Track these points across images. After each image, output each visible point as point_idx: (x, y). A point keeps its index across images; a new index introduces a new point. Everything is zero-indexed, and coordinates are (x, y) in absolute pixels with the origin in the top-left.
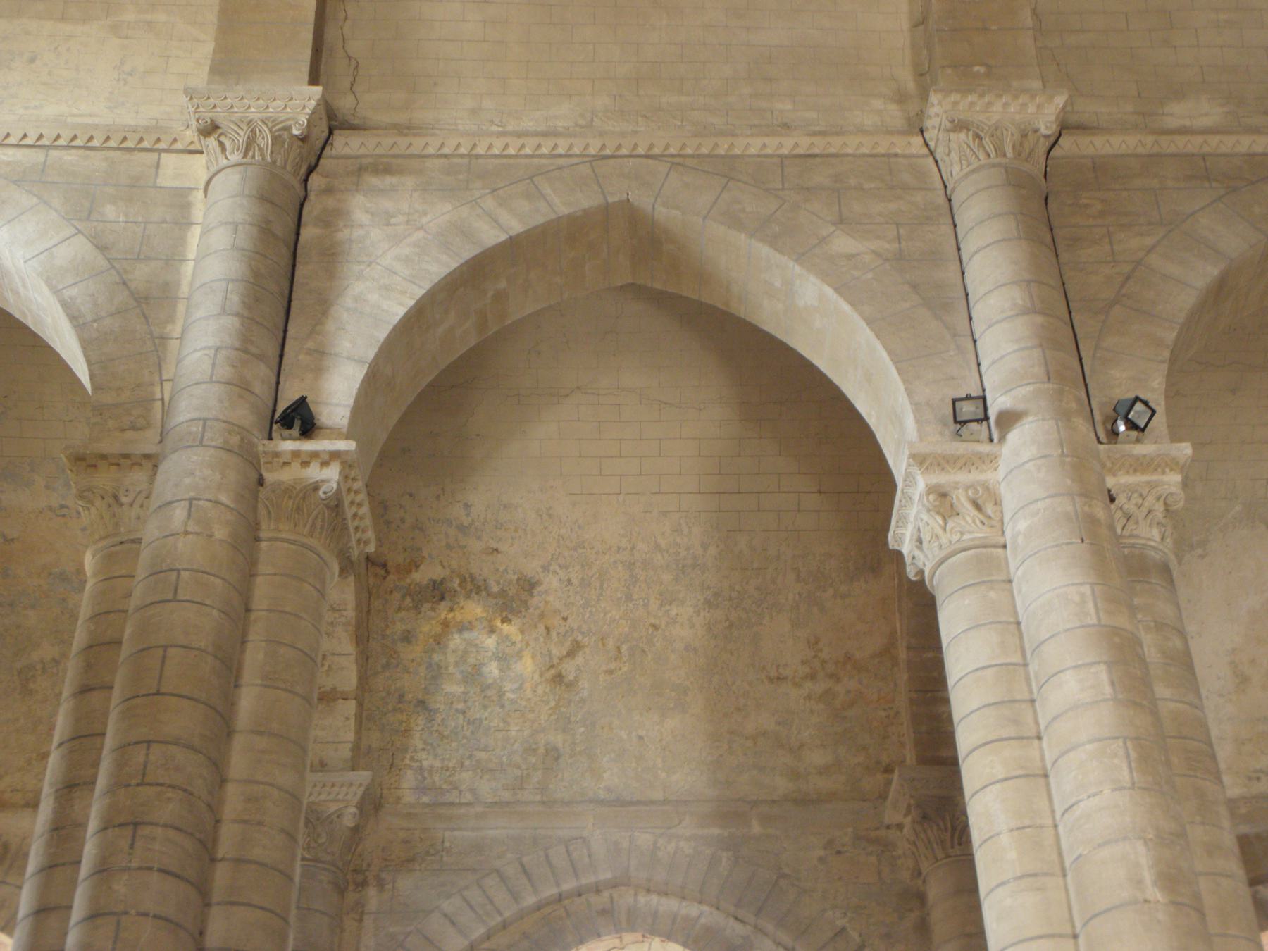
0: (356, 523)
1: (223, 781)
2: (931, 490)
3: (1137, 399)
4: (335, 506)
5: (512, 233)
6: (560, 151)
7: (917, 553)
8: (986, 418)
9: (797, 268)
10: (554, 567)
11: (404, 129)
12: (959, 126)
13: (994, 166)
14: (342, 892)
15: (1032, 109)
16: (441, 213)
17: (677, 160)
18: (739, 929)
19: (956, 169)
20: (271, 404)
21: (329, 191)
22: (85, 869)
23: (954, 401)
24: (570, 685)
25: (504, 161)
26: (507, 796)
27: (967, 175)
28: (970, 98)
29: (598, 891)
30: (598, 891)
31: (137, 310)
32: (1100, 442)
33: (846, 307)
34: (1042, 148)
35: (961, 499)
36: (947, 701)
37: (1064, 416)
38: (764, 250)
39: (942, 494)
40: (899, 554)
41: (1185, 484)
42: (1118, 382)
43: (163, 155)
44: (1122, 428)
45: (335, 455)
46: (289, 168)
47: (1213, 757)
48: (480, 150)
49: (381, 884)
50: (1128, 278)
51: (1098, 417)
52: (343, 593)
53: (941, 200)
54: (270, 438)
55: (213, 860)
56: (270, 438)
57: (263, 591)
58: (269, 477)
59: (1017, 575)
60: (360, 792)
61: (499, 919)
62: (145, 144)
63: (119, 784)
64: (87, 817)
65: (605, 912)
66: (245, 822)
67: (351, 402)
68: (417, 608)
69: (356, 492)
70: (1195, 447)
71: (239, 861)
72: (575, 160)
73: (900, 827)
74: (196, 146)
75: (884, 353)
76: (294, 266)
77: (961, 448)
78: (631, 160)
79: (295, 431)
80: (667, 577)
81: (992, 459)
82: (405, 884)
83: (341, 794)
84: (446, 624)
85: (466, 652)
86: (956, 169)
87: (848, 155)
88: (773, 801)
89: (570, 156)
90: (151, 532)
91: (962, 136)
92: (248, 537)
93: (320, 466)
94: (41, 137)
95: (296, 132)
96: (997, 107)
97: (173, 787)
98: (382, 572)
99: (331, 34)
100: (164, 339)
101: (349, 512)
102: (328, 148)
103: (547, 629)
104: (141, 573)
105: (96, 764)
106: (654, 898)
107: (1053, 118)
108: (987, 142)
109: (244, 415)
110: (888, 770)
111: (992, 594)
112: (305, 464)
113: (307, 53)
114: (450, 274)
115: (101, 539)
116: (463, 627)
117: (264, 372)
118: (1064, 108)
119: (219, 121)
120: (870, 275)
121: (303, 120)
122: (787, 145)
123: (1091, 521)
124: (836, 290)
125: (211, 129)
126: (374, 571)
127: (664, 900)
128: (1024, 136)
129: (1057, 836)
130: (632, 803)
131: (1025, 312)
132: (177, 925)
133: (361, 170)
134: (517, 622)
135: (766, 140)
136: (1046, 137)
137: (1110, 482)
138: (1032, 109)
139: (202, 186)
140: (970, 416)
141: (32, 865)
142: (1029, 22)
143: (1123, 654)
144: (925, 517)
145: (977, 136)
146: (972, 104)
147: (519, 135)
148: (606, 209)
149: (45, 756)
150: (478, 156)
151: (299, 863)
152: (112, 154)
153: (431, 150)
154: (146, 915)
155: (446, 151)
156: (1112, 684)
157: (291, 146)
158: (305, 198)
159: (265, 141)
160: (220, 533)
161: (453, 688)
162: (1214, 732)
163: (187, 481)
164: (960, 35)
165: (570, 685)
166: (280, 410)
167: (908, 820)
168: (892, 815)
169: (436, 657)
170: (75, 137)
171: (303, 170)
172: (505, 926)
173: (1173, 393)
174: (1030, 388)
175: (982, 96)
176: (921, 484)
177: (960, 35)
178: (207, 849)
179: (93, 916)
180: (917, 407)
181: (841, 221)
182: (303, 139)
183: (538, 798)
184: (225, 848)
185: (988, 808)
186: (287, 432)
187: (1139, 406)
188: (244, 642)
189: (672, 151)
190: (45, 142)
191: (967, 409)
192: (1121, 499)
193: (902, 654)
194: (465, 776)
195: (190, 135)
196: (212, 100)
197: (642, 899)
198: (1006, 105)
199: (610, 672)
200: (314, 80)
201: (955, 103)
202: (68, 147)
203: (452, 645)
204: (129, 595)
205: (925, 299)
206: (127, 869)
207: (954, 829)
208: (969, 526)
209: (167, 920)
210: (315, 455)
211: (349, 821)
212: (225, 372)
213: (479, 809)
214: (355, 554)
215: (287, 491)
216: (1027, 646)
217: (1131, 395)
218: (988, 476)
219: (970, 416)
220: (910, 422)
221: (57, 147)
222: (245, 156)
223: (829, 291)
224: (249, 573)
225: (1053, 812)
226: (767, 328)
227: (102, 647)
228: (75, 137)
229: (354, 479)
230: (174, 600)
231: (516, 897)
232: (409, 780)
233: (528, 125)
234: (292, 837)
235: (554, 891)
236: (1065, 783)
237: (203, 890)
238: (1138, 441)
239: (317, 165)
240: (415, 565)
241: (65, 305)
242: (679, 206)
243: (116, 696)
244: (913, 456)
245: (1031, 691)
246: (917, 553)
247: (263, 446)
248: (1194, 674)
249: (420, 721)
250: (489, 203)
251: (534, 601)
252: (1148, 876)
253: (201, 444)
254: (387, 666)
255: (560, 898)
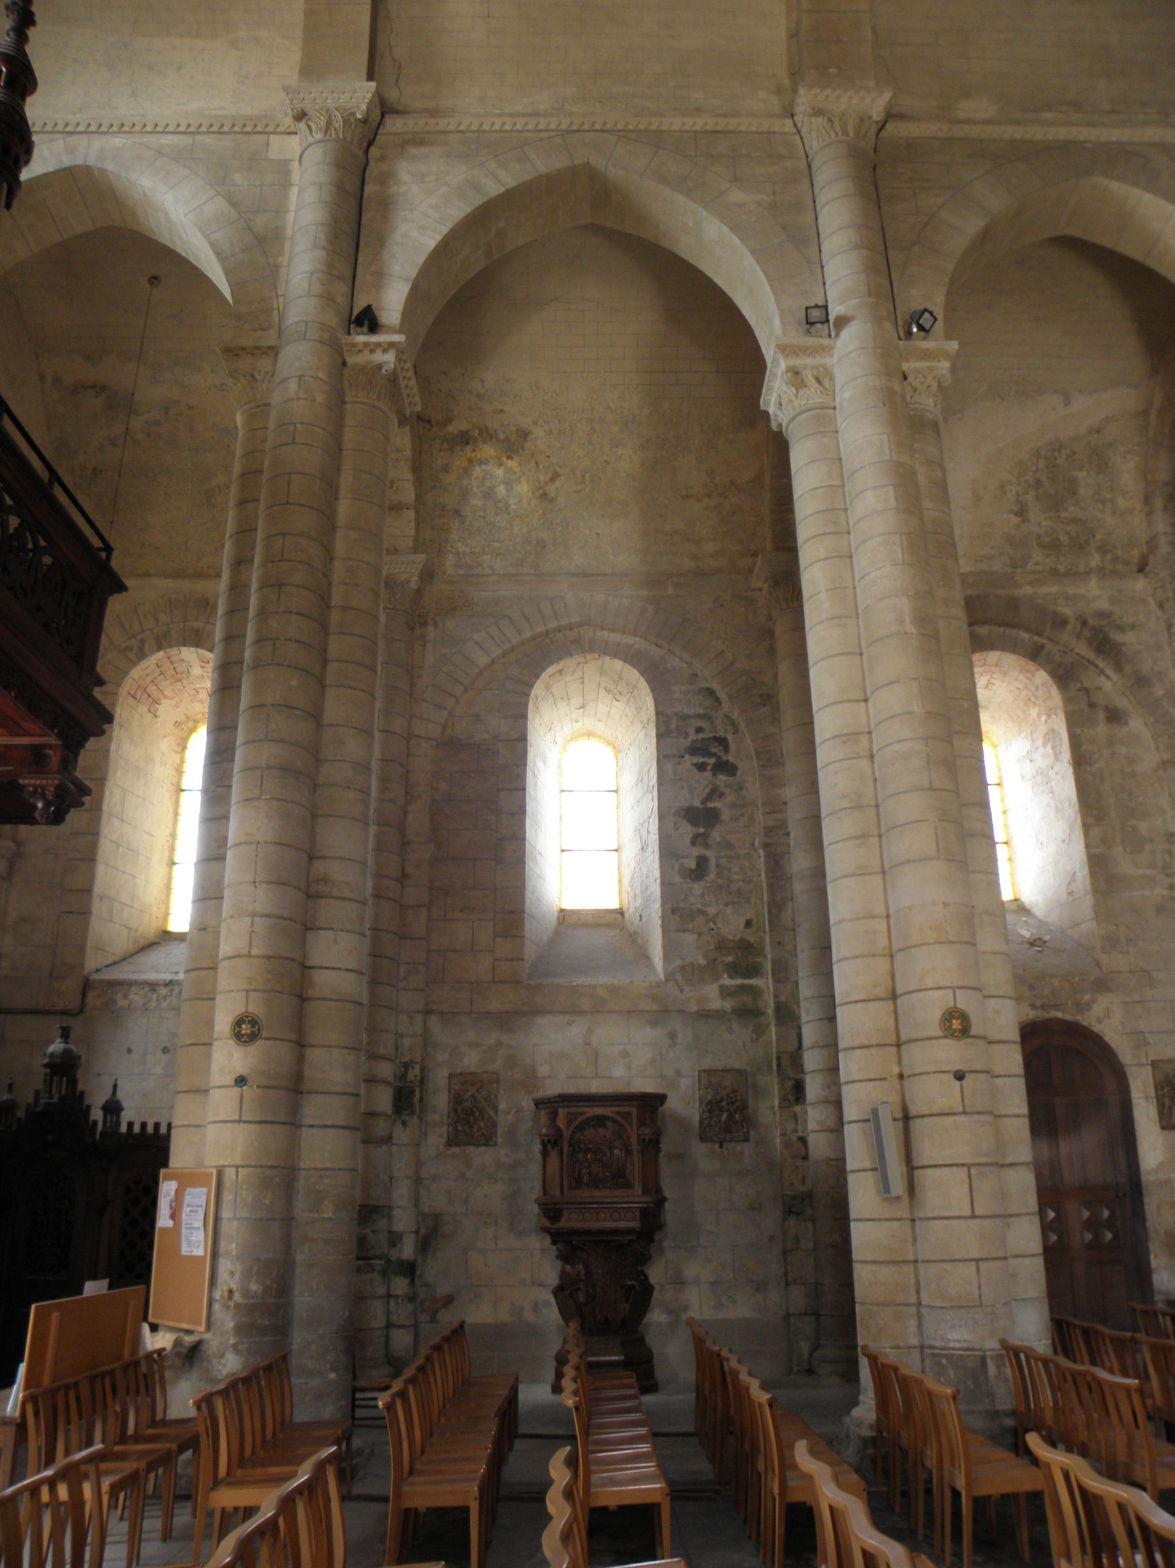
0: (408, 391)
1: (332, 559)
2: (789, 369)
3: (926, 310)
4: (393, 379)
5: (508, 187)
6: (541, 127)
7: (779, 413)
8: (827, 321)
9: (705, 213)
10: (541, 422)
11: (433, 113)
12: (818, 112)
13: (841, 142)
14: (412, 629)
15: (868, 101)
16: (459, 173)
17: (622, 134)
18: (658, 651)
19: (815, 144)
20: (348, 310)
21: (383, 158)
22: (252, 612)
23: (807, 308)
24: (552, 500)
25: (502, 135)
26: (512, 570)
27: (822, 149)
28: (827, 92)
29: (571, 629)
30: (571, 629)
31: (259, 246)
32: (900, 339)
33: (737, 241)
34: (873, 131)
35: (808, 376)
36: (792, 511)
37: (877, 320)
38: (683, 200)
39: (796, 373)
40: (767, 413)
41: (953, 370)
42: (914, 298)
43: (271, 136)
44: (915, 330)
45: (392, 345)
46: (355, 142)
47: (954, 546)
48: (486, 127)
49: (436, 625)
50: (925, 227)
51: (900, 322)
52: (402, 440)
53: (804, 166)
54: (349, 334)
55: (329, 607)
56: (349, 334)
57: (350, 437)
58: (350, 360)
59: (842, 426)
60: (420, 568)
61: (509, 645)
62: (259, 129)
63: (267, 561)
64: (251, 580)
65: (576, 641)
66: (346, 584)
67: (401, 308)
68: (451, 449)
69: (407, 370)
70: (960, 344)
71: (345, 608)
72: (553, 134)
73: (760, 590)
74: (293, 129)
75: (762, 274)
76: (360, 213)
77: (809, 341)
78: (591, 134)
79: (365, 329)
80: (615, 429)
81: (829, 349)
82: (450, 624)
83: (408, 569)
84: (470, 460)
85: (484, 479)
86: (815, 144)
87: (740, 132)
88: (682, 574)
89: (548, 131)
90: (276, 398)
91: (820, 120)
92: (338, 400)
93: (383, 351)
94: (189, 125)
95: (359, 116)
96: (845, 99)
97: (300, 562)
98: (428, 426)
99: (381, 44)
100: (277, 267)
101: (403, 383)
102: (381, 128)
103: (537, 463)
104: (272, 425)
105: (253, 549)
106: (606, 633)
107: (881, 108)
108: (836, 124)
109: (331, 318)
110: (755, 554)
111: (825, 440)
112: (372, 351)
113: (365, 57)
114: (466, 217)
115: (246, 404)
116: (481, 462)
117: (343, 288)
118: (889, 102)
119: (310, 111)
120: (754, 219)
121: (364, 107)
122: (699, 123)
123: (891, 392)
124: (731, 229)
125: (301, 116)
126: (422, 425)
127: (612, 634)
128: (862, 120)
129: (855, 593)
130: (592, 575)
131: (856, 248)
132: (310, 646)
133: (404, 144)
134: (516, 458)
135: (685, 120)
136: (877, 122)
137: (905, 366)
138: (868, 101)
139: (297, 157)
140: (817, 319)
141: (221, 611)
142: (870, 36)
143: (905, 481)
144: (784, 388)
145: (830, 120)
146: (827, 96)
147: (511, 115)
148: (573, 169)
149: (223, 546)
150: (484, 131)
151: (381, 610)
152: (237, 136)
153: (451, 128)
154: (290, 640)
155: (462, 128)
156: (896, 498)
157: (356, 126)
158: (367, 164)
159: (338, 123)
160: (320, 398)
161: (477, 502)
162: (957, 532)
163: (297, 364)
164: (820, 49)
165: (552, 500)
166: (356, 312)
167: (766, 586)
168: (756, 583)
169: (465, 482)
170: (211, 125)
171: (365, 144)
172: (513, 649)
173: (949, 307)
174: (857, 301)
175: (834, 90)
176: (783, 366)
177: (820, 49)
178: (324, 599)
179: (259, 641)
180: (782, 312)
181: (735, 179)
182: (364, 121)
183: (533, 572)
184: (336, 600)
185: (815, 578)
186: (359, 330)
187: (926, 315)
188: (339, 470)
189: (619, 127)
190: (192, 129)
191: (815, 314)
192: (911, 379)
193: (767, 480)
194: (486, 558)
195: (288, 120)
196: (302, 95)
197: (598, 634)
198: (851, 98)
199: (578, 492)
200: (370, 77)
201: (816, 96)
202: (208, 132)
203: (475, 474)
204: (265, 441)
205: (789, 237)
206: (277, 613)
207: (794, 591)
208: (813, 395)
209: (304, 643)
210: (378, 345)
211: (413, 585)
212: (317, 289)
213: (495, 578)
214: (408, 412)
215: (362, 369)
216: (845, 474)
217: (921, 308)
218: (827, 361)
219: (817, 319)
220: (777, 322)
221: (200, 133)
222: (325, 134)
223: (726, 229)
224: (340, 425)
225: (854, 579)
226: (683, 256)
227: (251, 474)
228: (211, 125)
229: (405, 362)
230: (293, 443)
231: (519, 632)
232: (450, 560)
233: (520, 108)
234: (376, 594)
235: (543, 628)
236: (862, 561)
237: (324, 626)
238: (924, 339)
239: (374, 139)
240: (448, 421)
241: (212, 245)
242: (624, 167)
243: (262, 506)
244: (778, 346)
245: (845, 503)
246: (779, 413)
247: (345, 339)
248: (947, 494)
249: (456, 523)
250: (492, 165)
251: (528, 445)
252: (908, 618)
253: (305, 339)
254: (434, 487)
255: (547, 633)
